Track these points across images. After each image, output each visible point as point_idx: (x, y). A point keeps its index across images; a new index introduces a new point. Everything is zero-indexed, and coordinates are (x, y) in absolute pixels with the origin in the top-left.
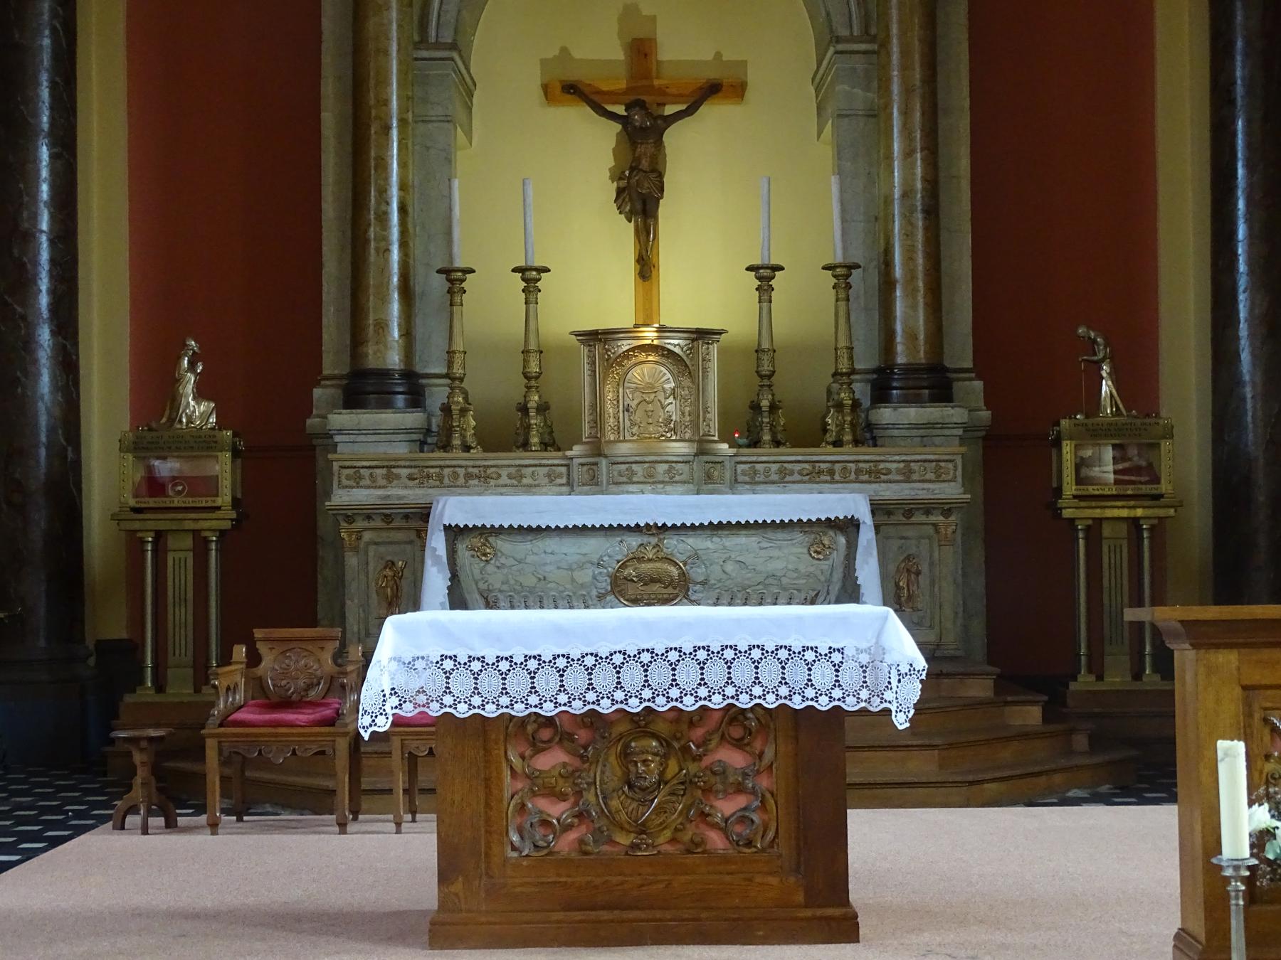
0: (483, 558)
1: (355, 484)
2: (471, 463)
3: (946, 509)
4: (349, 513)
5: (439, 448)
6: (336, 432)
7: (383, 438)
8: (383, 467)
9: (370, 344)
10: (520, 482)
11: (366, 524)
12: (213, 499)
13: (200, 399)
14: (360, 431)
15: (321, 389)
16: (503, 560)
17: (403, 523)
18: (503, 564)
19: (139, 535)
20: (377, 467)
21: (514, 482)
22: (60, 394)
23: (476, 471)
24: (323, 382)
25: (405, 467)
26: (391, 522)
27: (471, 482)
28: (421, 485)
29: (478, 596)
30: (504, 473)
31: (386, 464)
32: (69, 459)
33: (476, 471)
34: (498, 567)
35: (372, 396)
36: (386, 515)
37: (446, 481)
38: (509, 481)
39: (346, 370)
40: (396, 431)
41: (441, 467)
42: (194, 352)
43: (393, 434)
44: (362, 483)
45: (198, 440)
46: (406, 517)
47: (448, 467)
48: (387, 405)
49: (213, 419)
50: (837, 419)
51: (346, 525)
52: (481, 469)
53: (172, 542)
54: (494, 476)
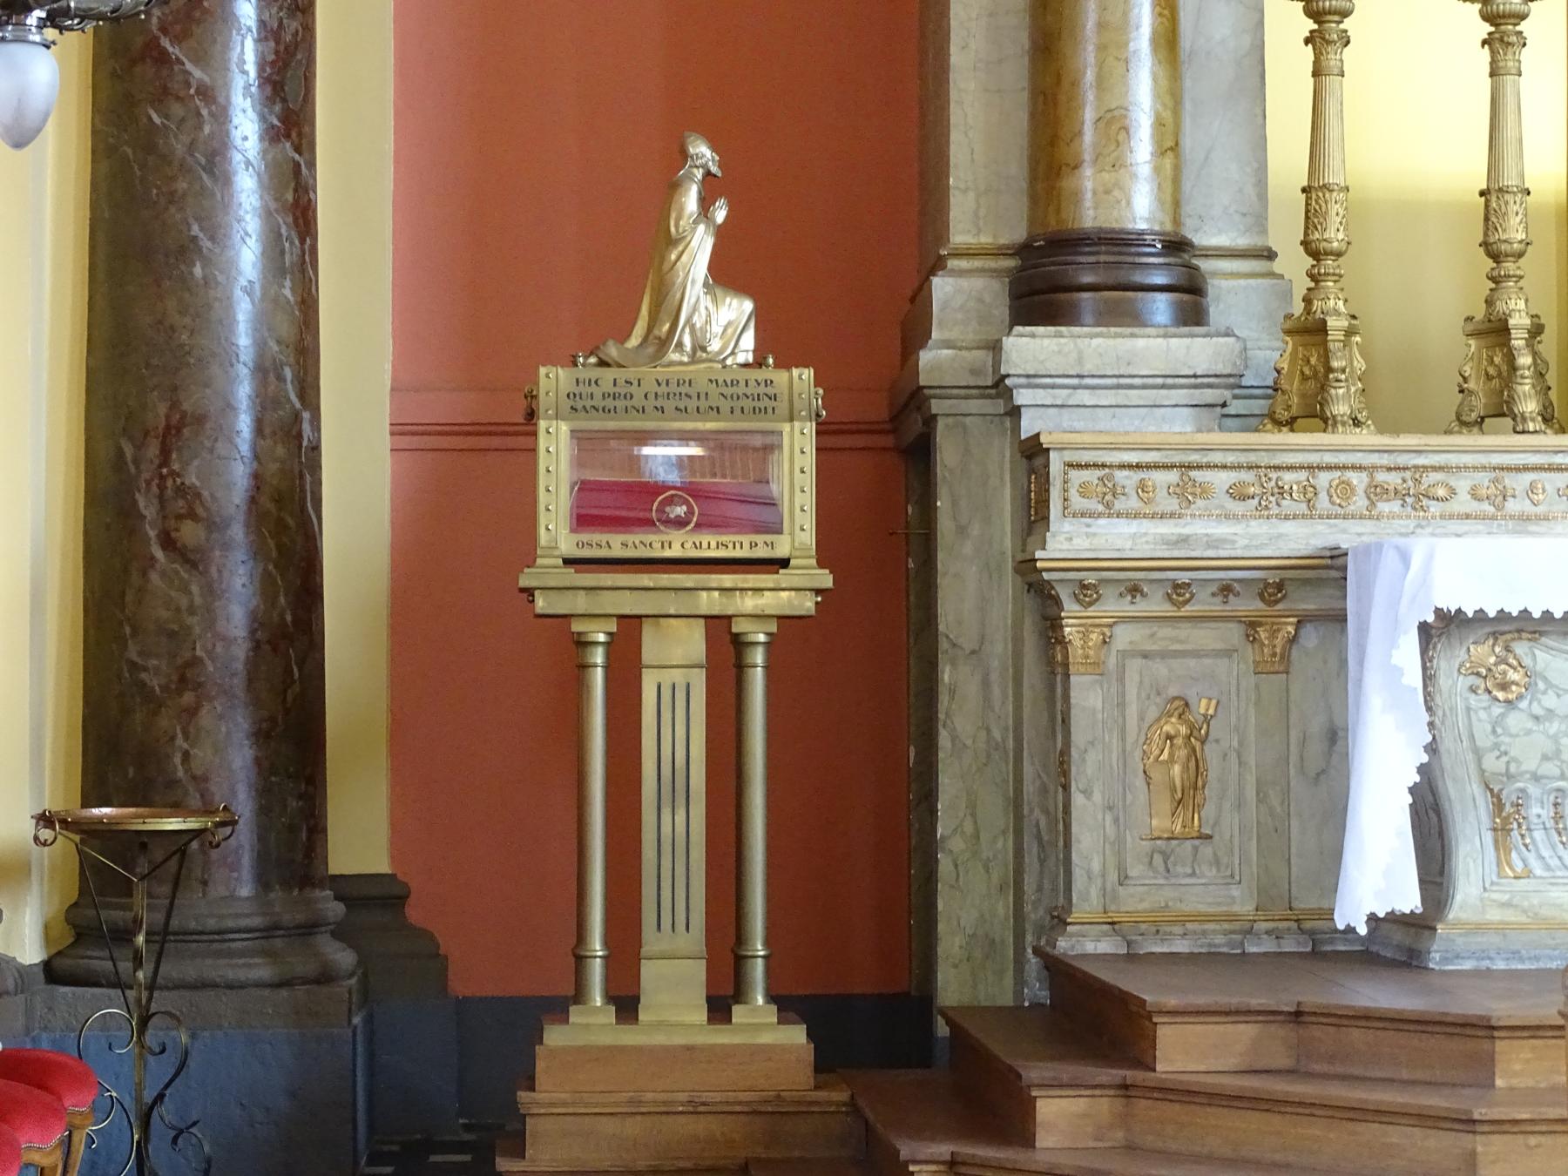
0: (1500, 695)
1: (1101, 508)
2: (1385, 460)
3: (541, 557)
4: (1091, 578)
5: (1279, 424)
6: (1023, 381)
7: (1134, 396)
8: (1171, 467)
9: (1086, 164)
10: (1108, 506)
11: (1125, 607)
12: (769, 538)
13: (719, 292)
14: (1080, 380)
15: (950, 280)
16: (1550, 700)
17: (1216, 606)
18: (1550, 711)
19: (577, 627)
20: (1156, 466)
21: (1487, 508)
22: (288, 283)
23: (1393, 479)
24: (952, 263)
25: (1224, 467)
26: (1187, 602)
27: (1384, 507)
28: (1262, 512)
29: (1477, 789)
30: (1463, 484)
31: (1177, 458)
32: (305, 443)
33: (1393, 479)
34: (1537, 718)
35: (1085, 295)
36: (1177, 586)
37: (1323, 502)
38: (1474, 507)
39: (1017, 233)
40: (1168, 381)
41: (1310, 468)
42: (708, 174)
43: (1163, 387)
44: (1119, 505)
45: (728, 391)
46: (1226, 590)
47: (1329, 468)
48: (1125, 316)
49: (748, 341)
50: (1491, 362)
51: (1076, 607)
52: (1408, 474)
53: (652, 646)
54: (1441, 492)
